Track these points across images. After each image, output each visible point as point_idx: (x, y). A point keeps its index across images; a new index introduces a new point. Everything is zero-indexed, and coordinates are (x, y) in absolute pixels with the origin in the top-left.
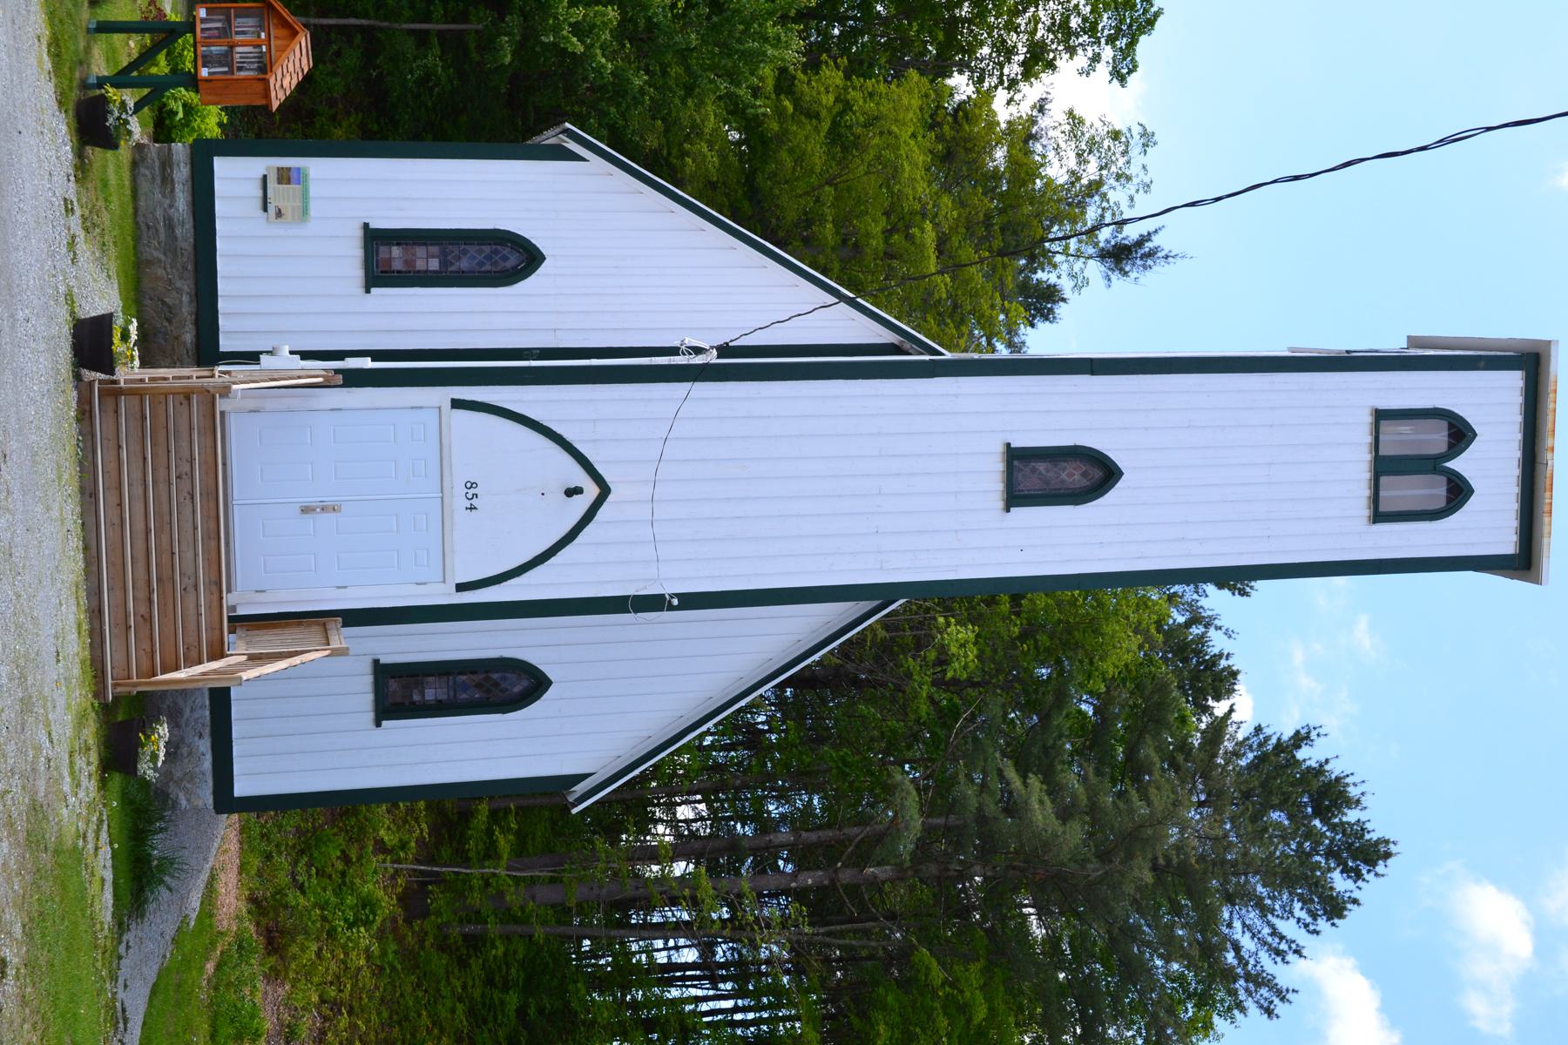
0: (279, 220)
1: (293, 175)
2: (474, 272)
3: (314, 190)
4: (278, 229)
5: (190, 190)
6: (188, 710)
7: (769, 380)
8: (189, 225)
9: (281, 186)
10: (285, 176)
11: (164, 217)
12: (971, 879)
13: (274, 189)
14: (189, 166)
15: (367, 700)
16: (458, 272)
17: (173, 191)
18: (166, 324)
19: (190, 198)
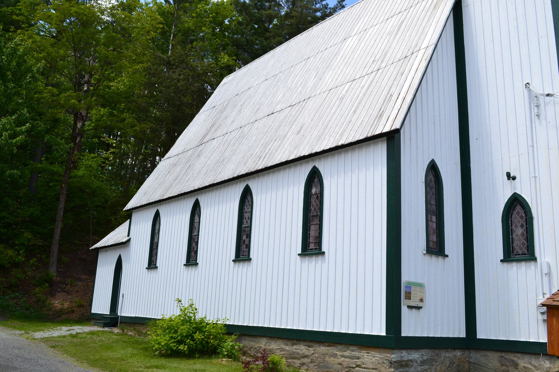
0: (424, 301)
1: (408, 290)
2: (436, 198)
3: (412, 280)
4: (427, 300)
5: (411, 350)
6: (131, 328)
7: (555, 27)
8: (423, 352)
9: (412, 298)
10: (408, 296)
11: (420, 366)
12: (121, 187)
13: (413, 302)
14: (402, 351)
15: (523, 266)
16: (436, 206)
17: (411, 361)
18: (455, 365)
19: (414, 351)
